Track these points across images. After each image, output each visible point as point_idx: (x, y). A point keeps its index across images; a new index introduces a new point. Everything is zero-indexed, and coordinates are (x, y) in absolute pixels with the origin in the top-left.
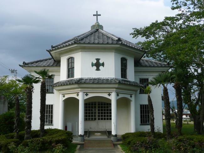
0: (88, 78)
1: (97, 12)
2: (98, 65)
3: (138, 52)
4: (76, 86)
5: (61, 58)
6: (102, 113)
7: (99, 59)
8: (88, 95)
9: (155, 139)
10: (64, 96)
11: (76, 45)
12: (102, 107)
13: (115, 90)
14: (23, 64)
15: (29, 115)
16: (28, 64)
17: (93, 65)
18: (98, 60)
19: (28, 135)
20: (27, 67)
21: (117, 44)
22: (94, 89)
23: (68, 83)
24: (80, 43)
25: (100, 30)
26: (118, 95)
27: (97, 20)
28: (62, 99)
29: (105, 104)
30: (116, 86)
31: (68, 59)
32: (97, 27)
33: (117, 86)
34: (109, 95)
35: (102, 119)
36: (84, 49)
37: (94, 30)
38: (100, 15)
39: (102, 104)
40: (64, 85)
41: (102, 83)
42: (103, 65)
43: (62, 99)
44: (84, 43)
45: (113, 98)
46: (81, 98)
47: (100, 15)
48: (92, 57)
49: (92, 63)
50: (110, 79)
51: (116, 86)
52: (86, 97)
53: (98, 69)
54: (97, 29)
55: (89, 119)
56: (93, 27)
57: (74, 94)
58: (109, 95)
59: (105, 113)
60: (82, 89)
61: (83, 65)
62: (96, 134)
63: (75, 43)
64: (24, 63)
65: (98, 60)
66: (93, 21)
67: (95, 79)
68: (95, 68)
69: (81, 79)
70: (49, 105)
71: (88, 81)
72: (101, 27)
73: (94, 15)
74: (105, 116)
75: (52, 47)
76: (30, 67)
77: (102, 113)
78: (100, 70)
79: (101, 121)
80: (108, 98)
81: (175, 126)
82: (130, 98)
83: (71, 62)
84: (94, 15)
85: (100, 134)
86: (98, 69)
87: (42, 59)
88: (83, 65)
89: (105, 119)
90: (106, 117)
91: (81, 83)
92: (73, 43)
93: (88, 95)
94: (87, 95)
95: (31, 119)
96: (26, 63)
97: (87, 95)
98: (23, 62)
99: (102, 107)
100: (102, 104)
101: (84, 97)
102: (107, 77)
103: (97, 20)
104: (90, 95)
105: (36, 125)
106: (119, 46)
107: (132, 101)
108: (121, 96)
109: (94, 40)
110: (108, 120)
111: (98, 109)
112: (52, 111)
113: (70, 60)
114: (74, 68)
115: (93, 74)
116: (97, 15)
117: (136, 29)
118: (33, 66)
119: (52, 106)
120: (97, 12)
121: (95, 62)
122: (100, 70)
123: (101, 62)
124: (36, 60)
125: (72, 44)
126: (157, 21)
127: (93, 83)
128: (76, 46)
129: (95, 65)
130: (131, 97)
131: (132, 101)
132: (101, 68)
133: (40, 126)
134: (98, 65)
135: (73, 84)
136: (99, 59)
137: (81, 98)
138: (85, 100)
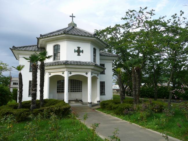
0: (72, 61)
1: (72, 14)
2: (79, 52)
3: (103, 44)
4: (64, 66)
5: (47, 46)
6: (73, 87)
7: (80, 47)
8: (71, 73)
9: (110, 104)
10: (50, 74)
11: (64, 35)
12: (73, 83)
13: (91, 70)
14: (13, 47)
15: (34, 88)
16: (17, 48)
17: (75, 51)
18: (79, 48)
19: (34, 105)
20: (16, 50)
21: (94, 37)
22: (76, 69)
23: (57, 64)
24: (68, 34)
25: (75, 27)
26: (92, 74)
27: (73, 20)
28: (48, 76)
29: (75, 81)
30: (93, 67)
31: (54, 46)
32: (73, 25)
33: (93, 68)
34: (87, 74)
35: (73, 91)
36: (69, 39)
37: (71, 27)
38: (75, 17)
39: (73, 81)
40: (53, 65)
41: (84, 65)
42: (82, 52)
43: (48, 76)
44: (71, 34)
45: (89, 76)
46: (66, 76)
47: (75, 17)
48: (74, 46)
49: (75, 50)
50: (87, 62)
51: (93, 67)
52: (70, 75)
53: (79, 55)
54: (73, 26)
55: (60, 92)
56: (70, 25)
57: (83, 73)
58: (87, 74)
59: (75, 87)
60: (67, 69)
61: (67, 51)
62: (71, 102)
63: (64, 33)
64: (13, 47)
65: (79, 48)
66: (70, 21)
67: (77, 62)
68: (77, 53)
69: (67, 62)
70: (103, 82)
71: (73, 63)
72: (76, 25)
73: (70, 16)
74: (75, 89)
75: (41, 35)
76: (19, 50)
77: (73, 87)
78: (80, 55)
79: (74, 92)
80: (86, 76)
81: (120, 98)
82: (97, 76)
83: (57, 49)
84: (70, 16)
85: (74, 102)
86: (79, 55)
87: (27, 45)
88: (67, 51)
89: (75, 91)
90: (78, 90)
91: (68, 64)
92: (63, 33)
93: (71, 73)
94: (70, 73)
95: (36, 92)
96: (15, 47)
97: (70, 73)
98: (13, 46)
99: (73, 83)
100: (73, 81)
101: (68, 75)
102: (85, 61)
103: (73, 20)
104: (73, 74)
105: (26, 97)
106: (95, 39)
107: (98, 79)
108: (94, 75)
109: (71, 33)
110: (78, 92)
111: (77, 84)
112: (104, 89)
113: (56, 48)
114: (60, 52)
115: (75, 58)
116: (72, 17)
117: (97, 30)
118: (22, 50)
119: (104, 82)
120: (72, 14)
121: (77, 49)
122: (80, 55)
123: (81, 49)
124: (23, 46)
125: (62, 34)
126: (110, 26)
127: (77, 65)
128: (65, 36)
129: (77, 52)
130: (98, 76)
131: (98, 79)
132: (81, 54)
133: (40, 97)
134: (79, 52)
135: (61, 65)
136: (80, 47)
137: (66, 76)
138: (69, 77)
